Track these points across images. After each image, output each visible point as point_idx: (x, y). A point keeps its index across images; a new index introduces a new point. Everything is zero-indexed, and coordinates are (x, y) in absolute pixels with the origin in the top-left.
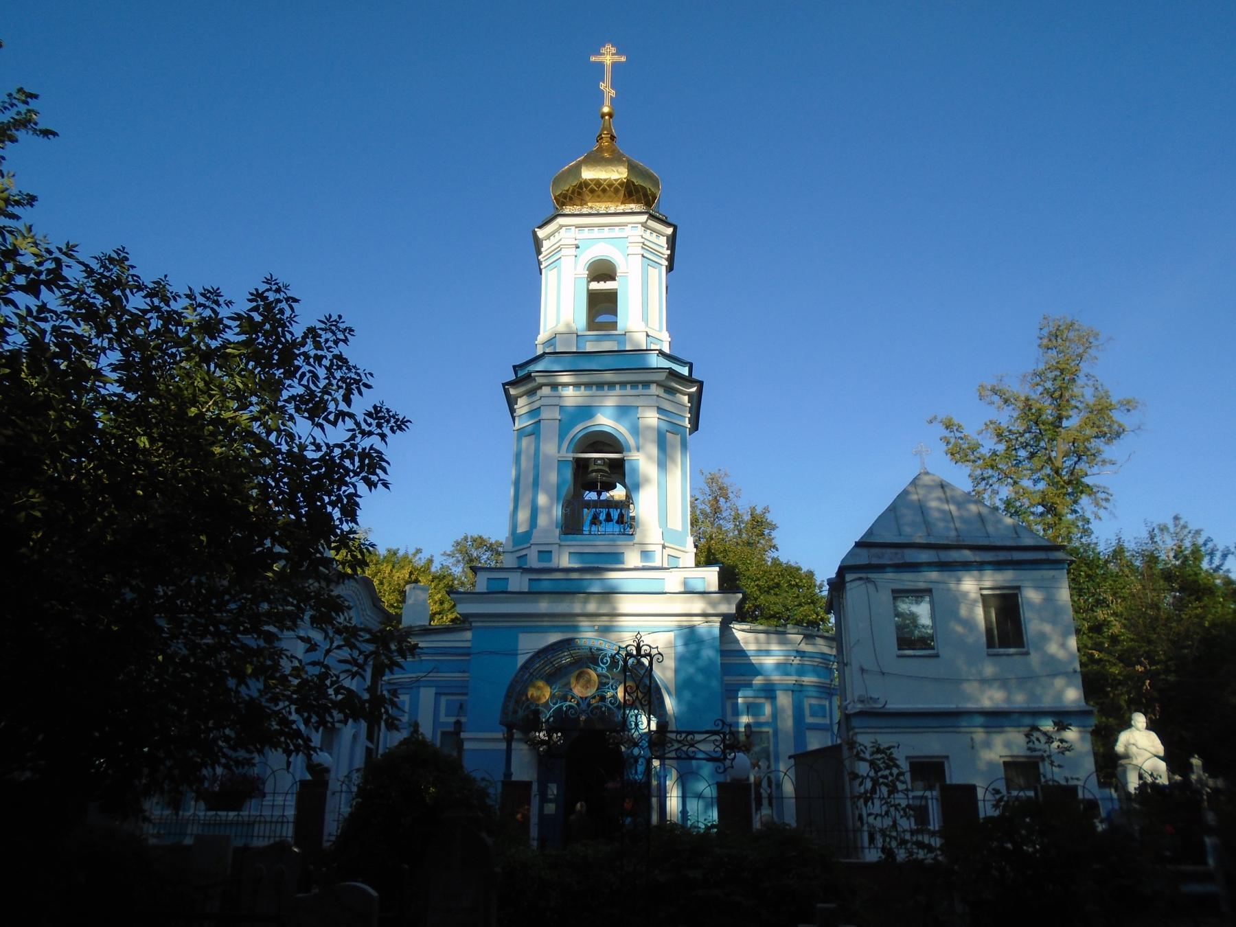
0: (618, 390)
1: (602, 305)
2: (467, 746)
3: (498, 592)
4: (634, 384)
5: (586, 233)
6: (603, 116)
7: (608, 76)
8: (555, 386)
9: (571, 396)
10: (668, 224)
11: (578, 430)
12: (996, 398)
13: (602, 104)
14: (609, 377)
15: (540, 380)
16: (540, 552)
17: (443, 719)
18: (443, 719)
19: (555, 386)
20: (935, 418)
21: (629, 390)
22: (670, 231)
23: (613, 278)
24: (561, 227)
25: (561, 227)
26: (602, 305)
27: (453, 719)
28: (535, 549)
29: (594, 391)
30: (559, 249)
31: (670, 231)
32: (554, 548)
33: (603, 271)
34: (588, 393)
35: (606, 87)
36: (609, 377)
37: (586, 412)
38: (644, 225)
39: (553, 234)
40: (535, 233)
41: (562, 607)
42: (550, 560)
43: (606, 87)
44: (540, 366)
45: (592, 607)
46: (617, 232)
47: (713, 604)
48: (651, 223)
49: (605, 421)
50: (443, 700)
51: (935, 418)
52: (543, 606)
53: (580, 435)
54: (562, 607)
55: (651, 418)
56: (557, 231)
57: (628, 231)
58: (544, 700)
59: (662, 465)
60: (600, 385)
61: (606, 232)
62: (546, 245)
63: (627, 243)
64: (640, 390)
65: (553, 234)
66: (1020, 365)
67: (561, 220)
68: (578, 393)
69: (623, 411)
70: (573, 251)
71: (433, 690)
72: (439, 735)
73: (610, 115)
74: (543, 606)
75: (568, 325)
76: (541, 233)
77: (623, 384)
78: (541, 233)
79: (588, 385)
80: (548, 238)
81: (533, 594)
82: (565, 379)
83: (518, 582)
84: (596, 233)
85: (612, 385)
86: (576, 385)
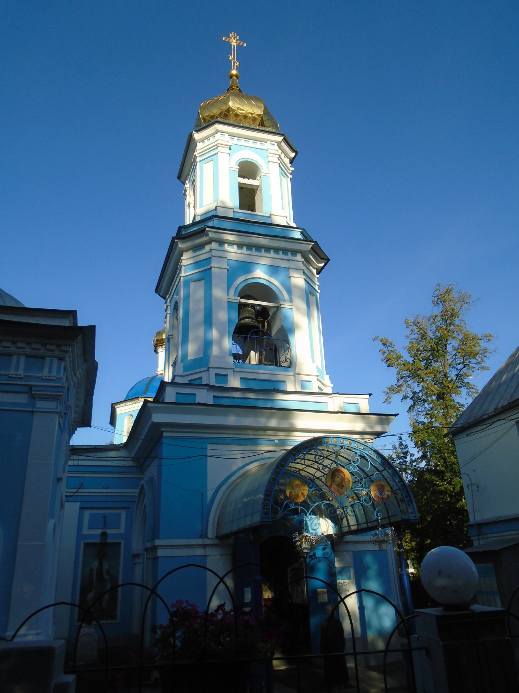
0: (272, 254)
1: (248, 197)
2: (161, 553)
3: (185, 404)
4: (285, 251)
5: (235, 141)
6: (231, 76)
7: (234, 52)
8: (221, 242)
9: (233, 252)
10: (293, 150)
11: (240, 281)
12: (415, 328)
13: (231, 69)
14: (264, 241)
15: (211, 235)
16: (217, 375)
17: (86, 531)
18: (86, 531)
19: (221, 242)
20: (378, 337)
21: (281, 255)
22: (293, 155)
23: (254, 178)
24: (217, 131)
25: (217, 131)
26: (248, 197)
27: (99, 532)
28: (213, 372)
29: (254, 252)
30: (217, 146)
31: (293, 155)
32: (229, 372)
33: (248, 170)
34: (248, 252)
35: (233, 58)
36: (264, 241)
37: (246, 267)
38: (279, 143)
39: (208, 138)
40: (191, 136)
41: (248, 421)
42: (227, 382)
43: (233, 58)
44: (210, 224)
45: (273, 423)
46: (258, 145)
47: (369, 424)
48: (283, 144)
49: (260, 274)
50: (87, 514)
51: (378, 337)
52: (232, 420)
53: (241, 286)
54: (248, 421)
55: (298, 280)
56: (213, 135)
57: (267, 146)
58: (301, 499)
59: (309, 315)
60: (258, 248)
61: (251, 143)
62: (199, 146)
63: (269, 154)
64: (289, 256)
65: (208, 138)
66: (426, 309)
67: (218, 126)
68: (239, 251)
69: (274, 270)
70: (227, 150)
71: (77, 505)
72: (82, 544)
73: (236, 76)
74: (232, 420)
75: (222, 202)
76: (197, 136)
77: (277, 250)
78: (197, 136)
79: (249, 247)
80: (203, 141)
81: (217, 407)
82: (230, 237)
83: (204, 397)
84: (243, 142)
85: (268, 249)
86: (240, 246)
